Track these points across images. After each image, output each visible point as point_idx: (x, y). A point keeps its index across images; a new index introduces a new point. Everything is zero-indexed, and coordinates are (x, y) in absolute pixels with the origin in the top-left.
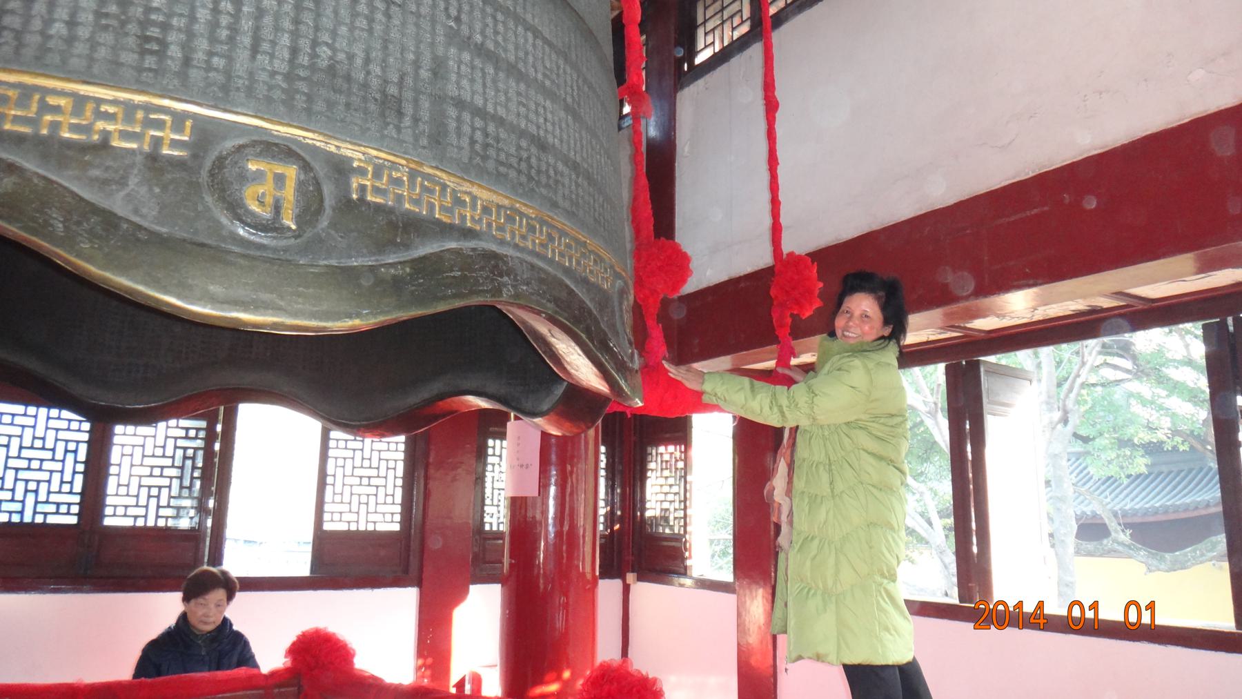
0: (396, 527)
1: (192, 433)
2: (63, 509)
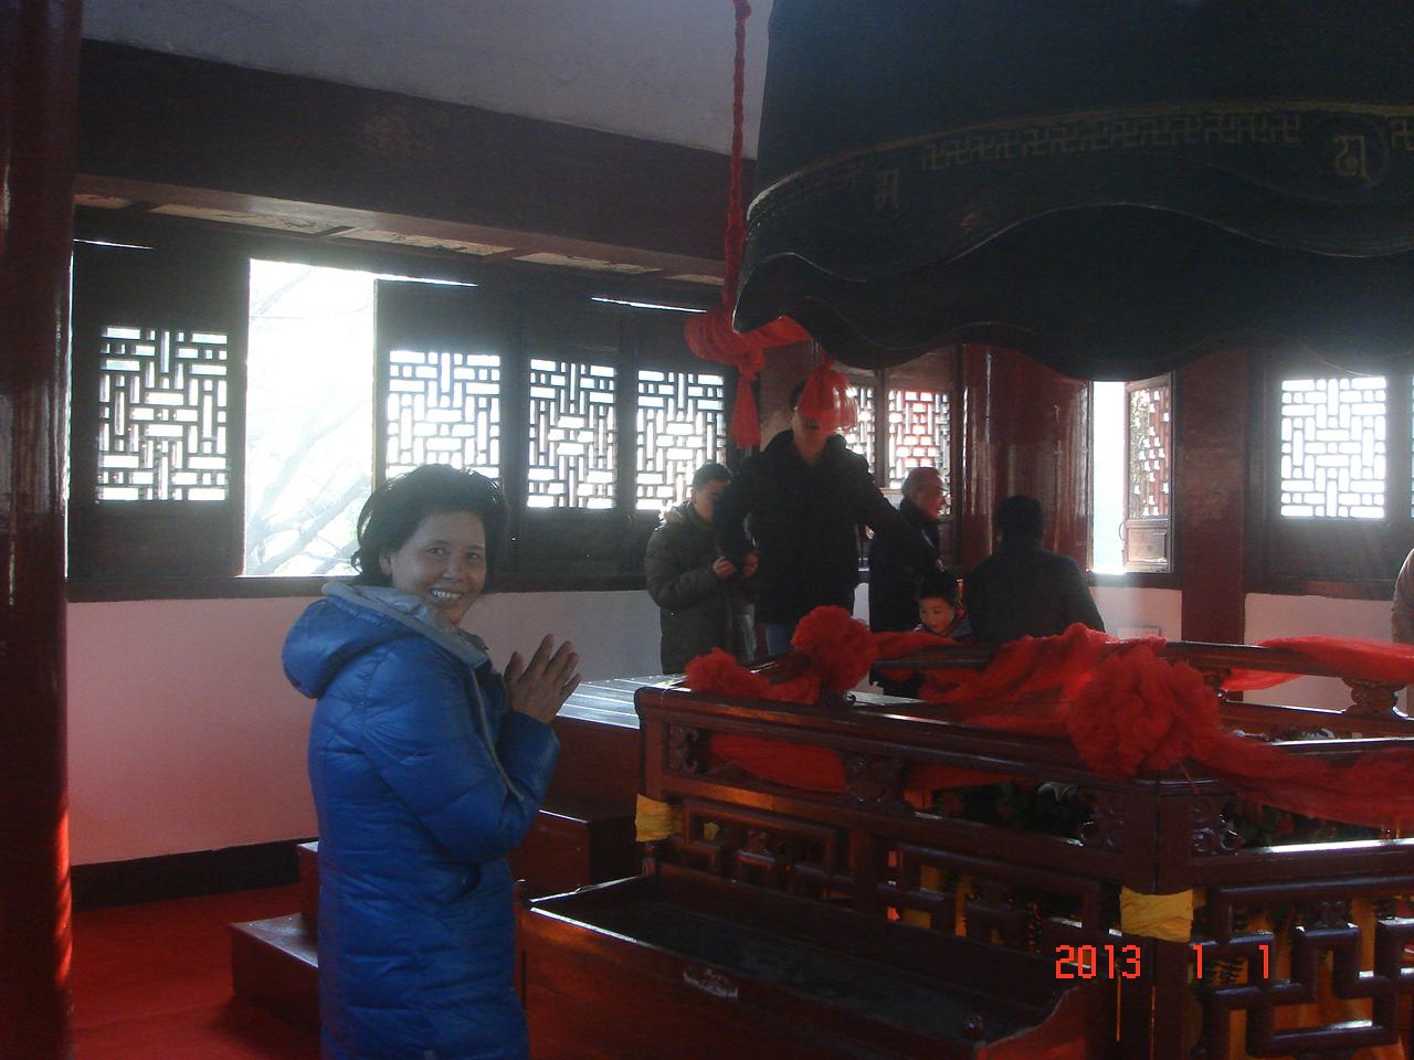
0: (1287, 385)
1: (407, 372)
2: (207, 479)
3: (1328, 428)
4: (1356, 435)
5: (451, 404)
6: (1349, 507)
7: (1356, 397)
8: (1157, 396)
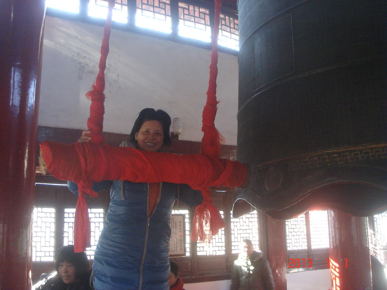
3: (45, 246)
4: (43, 230)
5: (241, 226)
6: (40, 257)
7: (43, 215)
8: (252, 268)
